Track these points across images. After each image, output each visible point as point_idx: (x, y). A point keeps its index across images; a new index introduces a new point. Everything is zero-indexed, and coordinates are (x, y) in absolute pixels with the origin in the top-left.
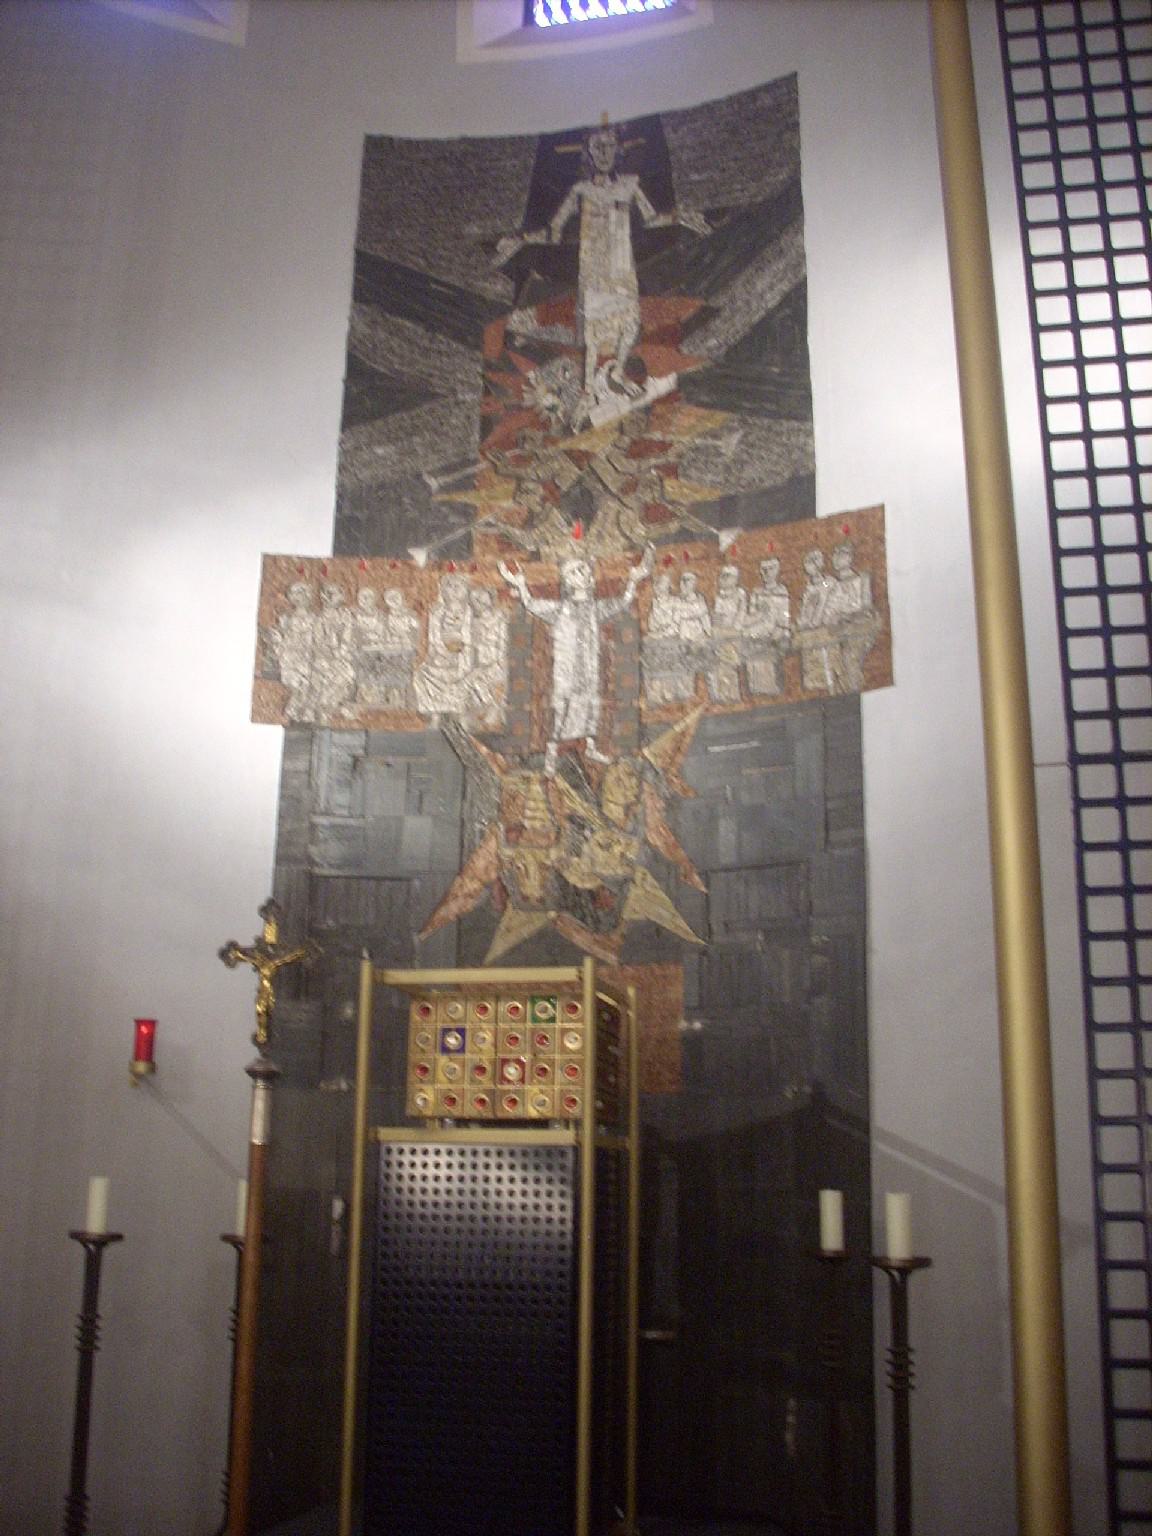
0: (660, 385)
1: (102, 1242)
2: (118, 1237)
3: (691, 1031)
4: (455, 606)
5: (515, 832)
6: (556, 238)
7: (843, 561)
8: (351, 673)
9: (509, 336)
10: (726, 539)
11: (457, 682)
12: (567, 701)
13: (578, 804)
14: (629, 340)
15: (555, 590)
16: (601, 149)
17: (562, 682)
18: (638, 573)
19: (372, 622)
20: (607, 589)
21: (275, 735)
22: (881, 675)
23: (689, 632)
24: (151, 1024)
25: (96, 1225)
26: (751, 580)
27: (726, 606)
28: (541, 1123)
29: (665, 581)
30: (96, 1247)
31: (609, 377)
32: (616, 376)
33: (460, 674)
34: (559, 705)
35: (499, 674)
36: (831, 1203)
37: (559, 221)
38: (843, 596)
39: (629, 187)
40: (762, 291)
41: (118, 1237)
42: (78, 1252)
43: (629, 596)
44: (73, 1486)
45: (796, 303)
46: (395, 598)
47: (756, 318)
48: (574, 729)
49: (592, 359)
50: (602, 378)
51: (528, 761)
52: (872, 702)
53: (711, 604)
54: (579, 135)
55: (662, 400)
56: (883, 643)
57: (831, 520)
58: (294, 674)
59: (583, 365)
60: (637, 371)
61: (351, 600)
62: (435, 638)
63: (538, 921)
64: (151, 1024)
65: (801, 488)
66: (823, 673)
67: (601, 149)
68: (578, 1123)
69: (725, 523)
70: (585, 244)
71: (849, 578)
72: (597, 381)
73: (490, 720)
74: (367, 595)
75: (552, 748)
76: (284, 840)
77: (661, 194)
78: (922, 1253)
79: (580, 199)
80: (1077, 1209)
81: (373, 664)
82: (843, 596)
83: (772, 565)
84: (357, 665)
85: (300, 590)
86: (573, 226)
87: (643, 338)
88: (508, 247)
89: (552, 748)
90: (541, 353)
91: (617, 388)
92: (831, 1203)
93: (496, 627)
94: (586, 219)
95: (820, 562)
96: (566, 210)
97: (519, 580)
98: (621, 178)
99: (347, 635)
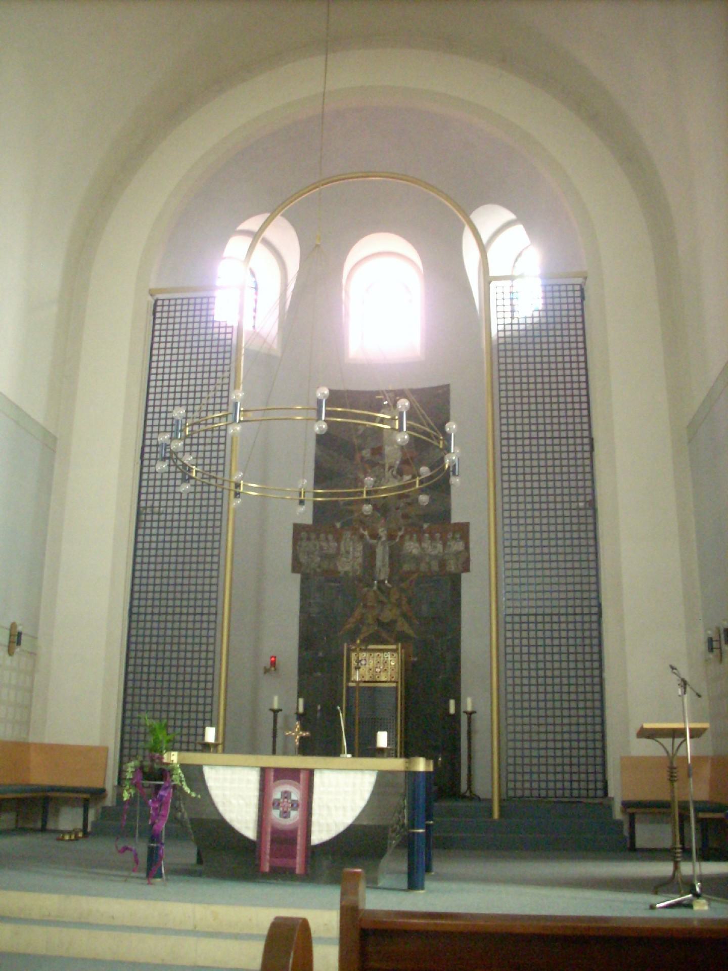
2: (281, 710)
3: (413, 661)
4: (348, 540)
7: (458, 536)
8: (319, 559)
10: (425, 526)
11: (349, 562)
12: (380, 570)
14: (398, 462)
15: (375, 536)
17: (379, 563)
18: (400, 533)
19: (324, 544)
20: (391, 537)
21: (298, 577)
22: (467, 569)
23: (415, 552)
24: (275, 657)
26: (432, 538)
27: (425, 545)
29: (407, 537)
30: (275, 712)
31: (392, 474)
32: (395, 473)
33: (349, 560)
35: (360, 560)
36: (452, 703)
38: (458, 546)
41: (281, 710)
42: (271, 714)
43: (398, 540)
46: (330, 537)
48: (382, 578)
51: (370, 585)
52: (464, 576)
53: (420, 544)
56: (467, 562)
58: (303, 558)
59: (384, 469)
60: (401, 473)
61: (318, 537)
62: (342, 549)
64: (275, 657)
65: (447, 514)
66: (452, 567)
69: (425, 522)
71: (459, 541)
73: (358, 573)
74: (322, 536)
78: (474, 710)
81: (325, 557)
82: (458, 546)
83: (438, 535)
84: (321, 557)
85: (304, 534)
91: (395, 477)
92: (452, 703)
93: (360, 547)
95: (451, 535)
97: (366, 533)
99: (318, 548)
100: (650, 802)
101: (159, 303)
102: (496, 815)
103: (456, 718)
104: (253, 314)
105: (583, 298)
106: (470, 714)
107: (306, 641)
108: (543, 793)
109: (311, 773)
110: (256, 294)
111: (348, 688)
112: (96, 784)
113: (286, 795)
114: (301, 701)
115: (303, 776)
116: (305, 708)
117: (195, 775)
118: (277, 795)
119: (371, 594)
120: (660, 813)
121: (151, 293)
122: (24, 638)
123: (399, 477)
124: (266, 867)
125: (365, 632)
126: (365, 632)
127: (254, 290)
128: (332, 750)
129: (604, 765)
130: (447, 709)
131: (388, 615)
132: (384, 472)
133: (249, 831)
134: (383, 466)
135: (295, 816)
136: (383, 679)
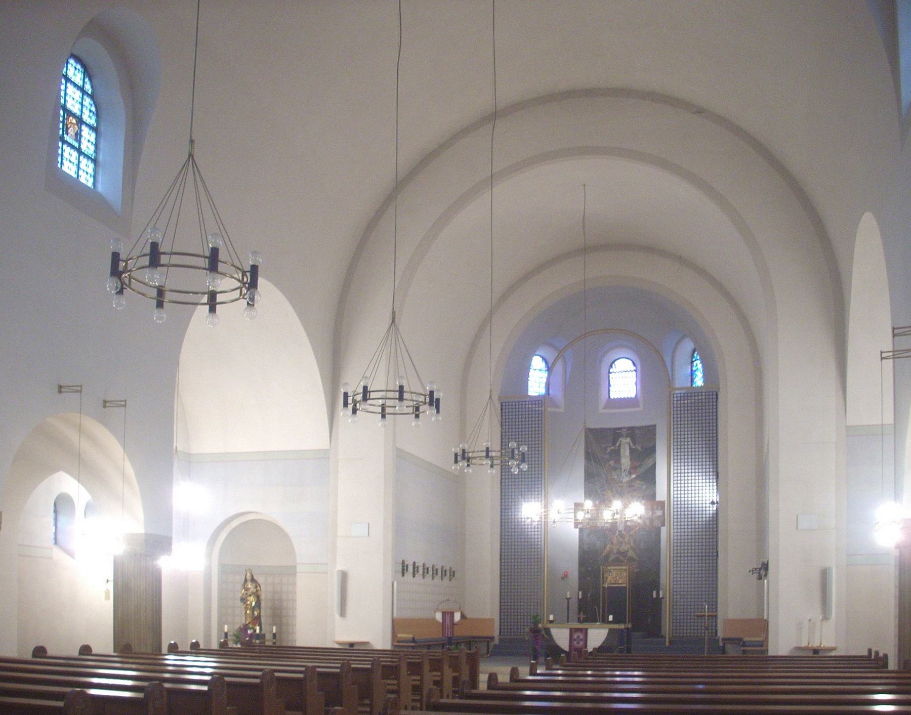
0: (633, 476)
1: (569, 599)
5: (612, 543)
6: (617, 448)
9: (610, 465)
13: (621, 540)
14: (628, 468)
16: (624, 432)
21: (577, 530)
25: (568, 597)
28: (621, 584)
30: (568, 599)
34: (618, 525)
36: (654, 593)
37: (617, 445)
39: (628, 440)
40: (649, 463)
42: (566, 601)
44: (899, 613)
45: (655, 464)
47: (648, 467)
49: (623, 471)
50: (624, 474)
54: (620, 429)
55: (633, 479)
57: (658, 502)
60: (630, 473)
63: (616, 556)
67: (624, 432)
68: (626, 583)
70: (621, 450)
72: (623, 474)
75: (617, 532)
76: (580, 545)
77: (634, 441)
79: (621, 441)
80: (671, 587)
86: (620, 445)
87: (631, 468)
88: (609, 450)
89: (617, 532)
90: (615, 469)
91: (627, 476)
92: (654, 593)
94: (622, 445)
96: (618, 443)
98: (627, 438)
100: (15, 660)
101: (504, 404)
102: (667, 644)
108: (681, 635)
109: (586, 630)
111: (604, 588)
112: (489, 635)
114: (580, 593)
115: (584, 631)
116: (583, 595)
118: (575, 637)
119: (615, 538)
120: (432, 642)
122: (456, 574)
123: (629, 476)
130: (652, 596)
132: (621, 473)
133: (567, 649)
134: (621, 469)
136: (620, 582)
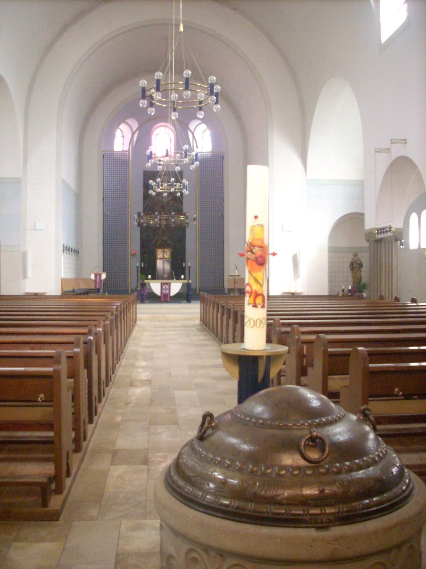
103: (184, 268)
104: (122, 145)
105: (223, 158)
106: (189, 267)
107: (142, 246)
109: (170, 284)
110: (123, 138)
113: (166, 287)
115: (169, 284)
117: (149, 284)
121: (102, 151)
124: (162, 300)
125: (158, 244)
126: (158, 244)
127: (122, 137)
128: (173, 279)
129: (223, 280)
131: (165, 238)
135: (167, 291)
